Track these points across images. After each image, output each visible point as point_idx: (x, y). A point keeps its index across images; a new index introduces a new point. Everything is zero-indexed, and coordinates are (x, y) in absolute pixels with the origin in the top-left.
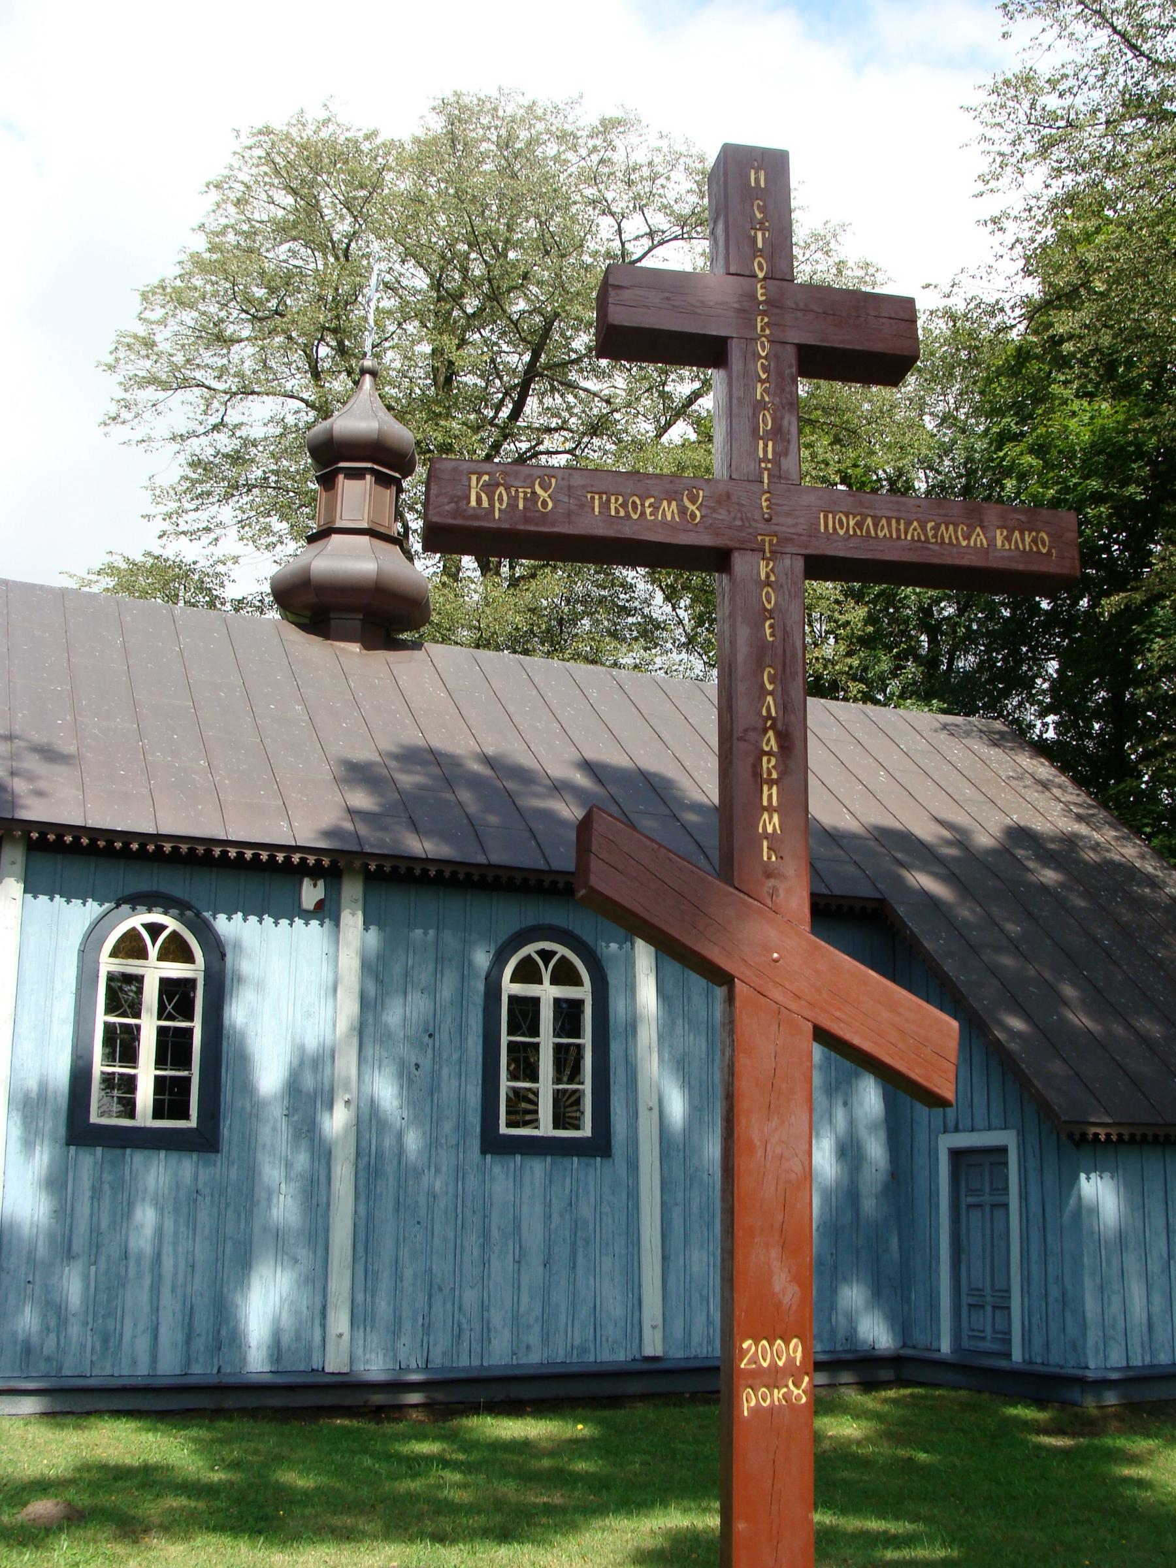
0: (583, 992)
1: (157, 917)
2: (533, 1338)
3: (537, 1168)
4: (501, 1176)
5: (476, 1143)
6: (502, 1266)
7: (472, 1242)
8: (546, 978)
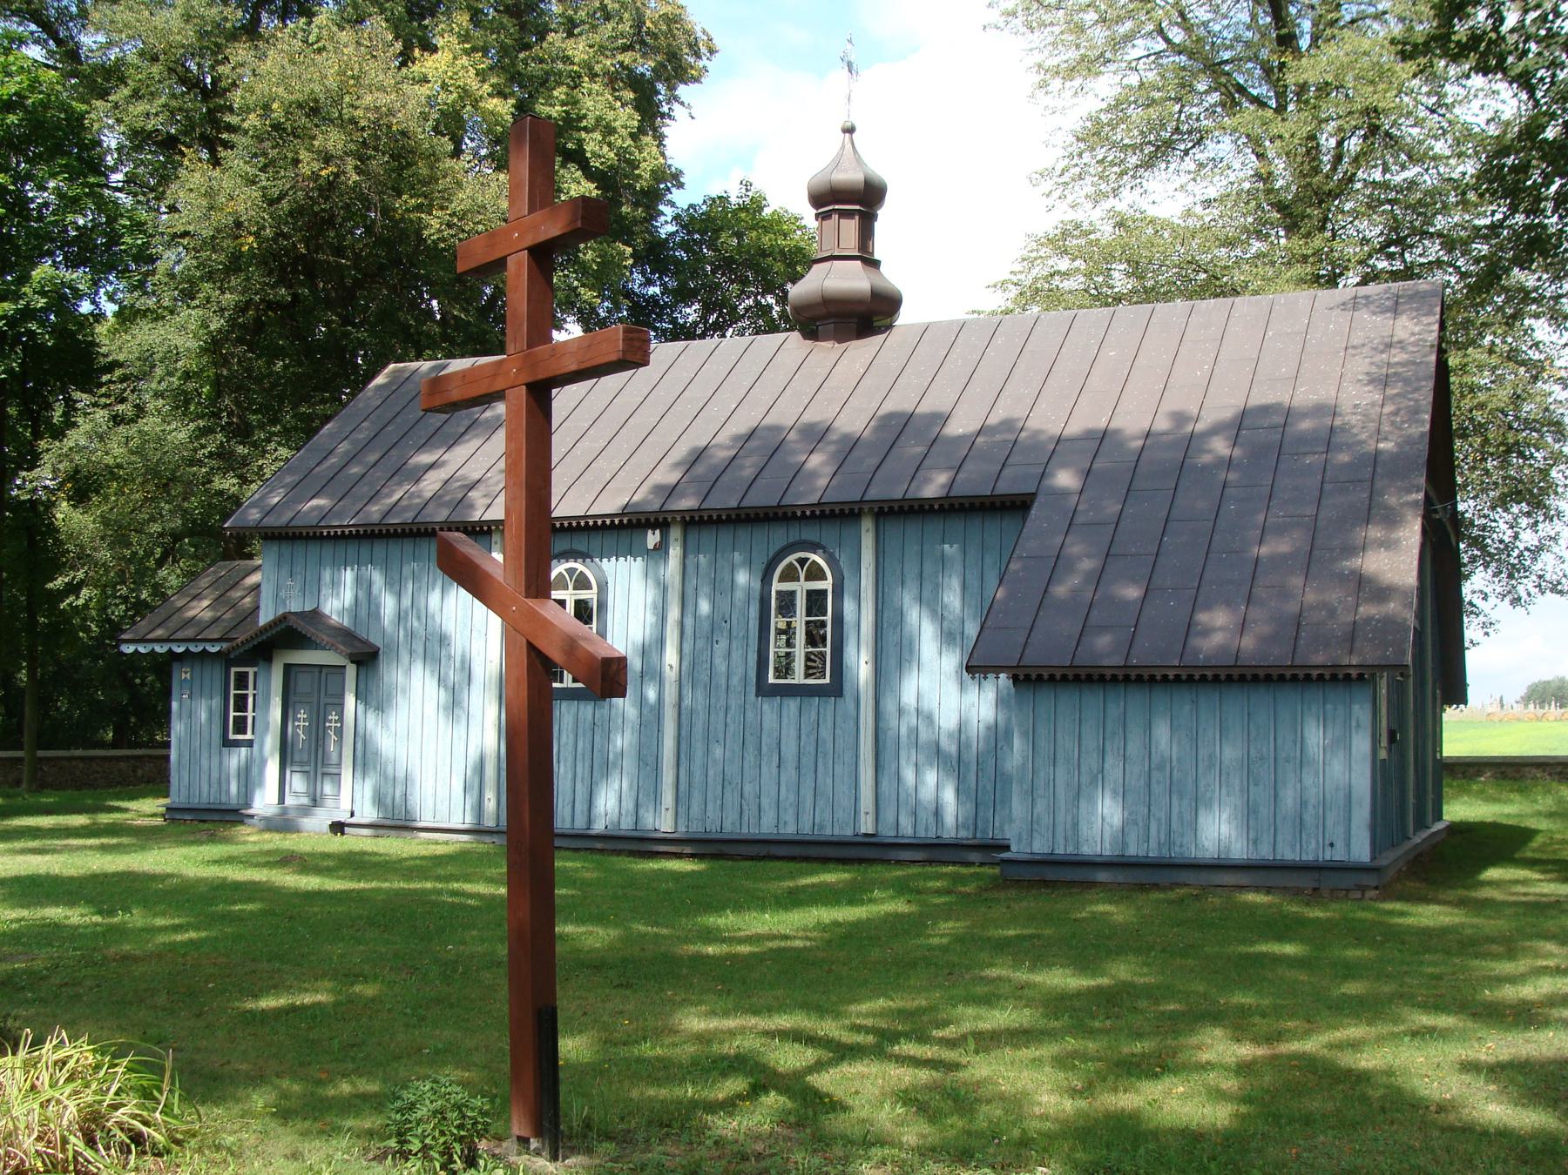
0: (826, 585)
1: (571, 564)
2: (789, 817)
3: (792, 705)
4: (769, 707)
5: (752, 689)
6: (769, 770)
7: (750, 758)
8: (571, 586)
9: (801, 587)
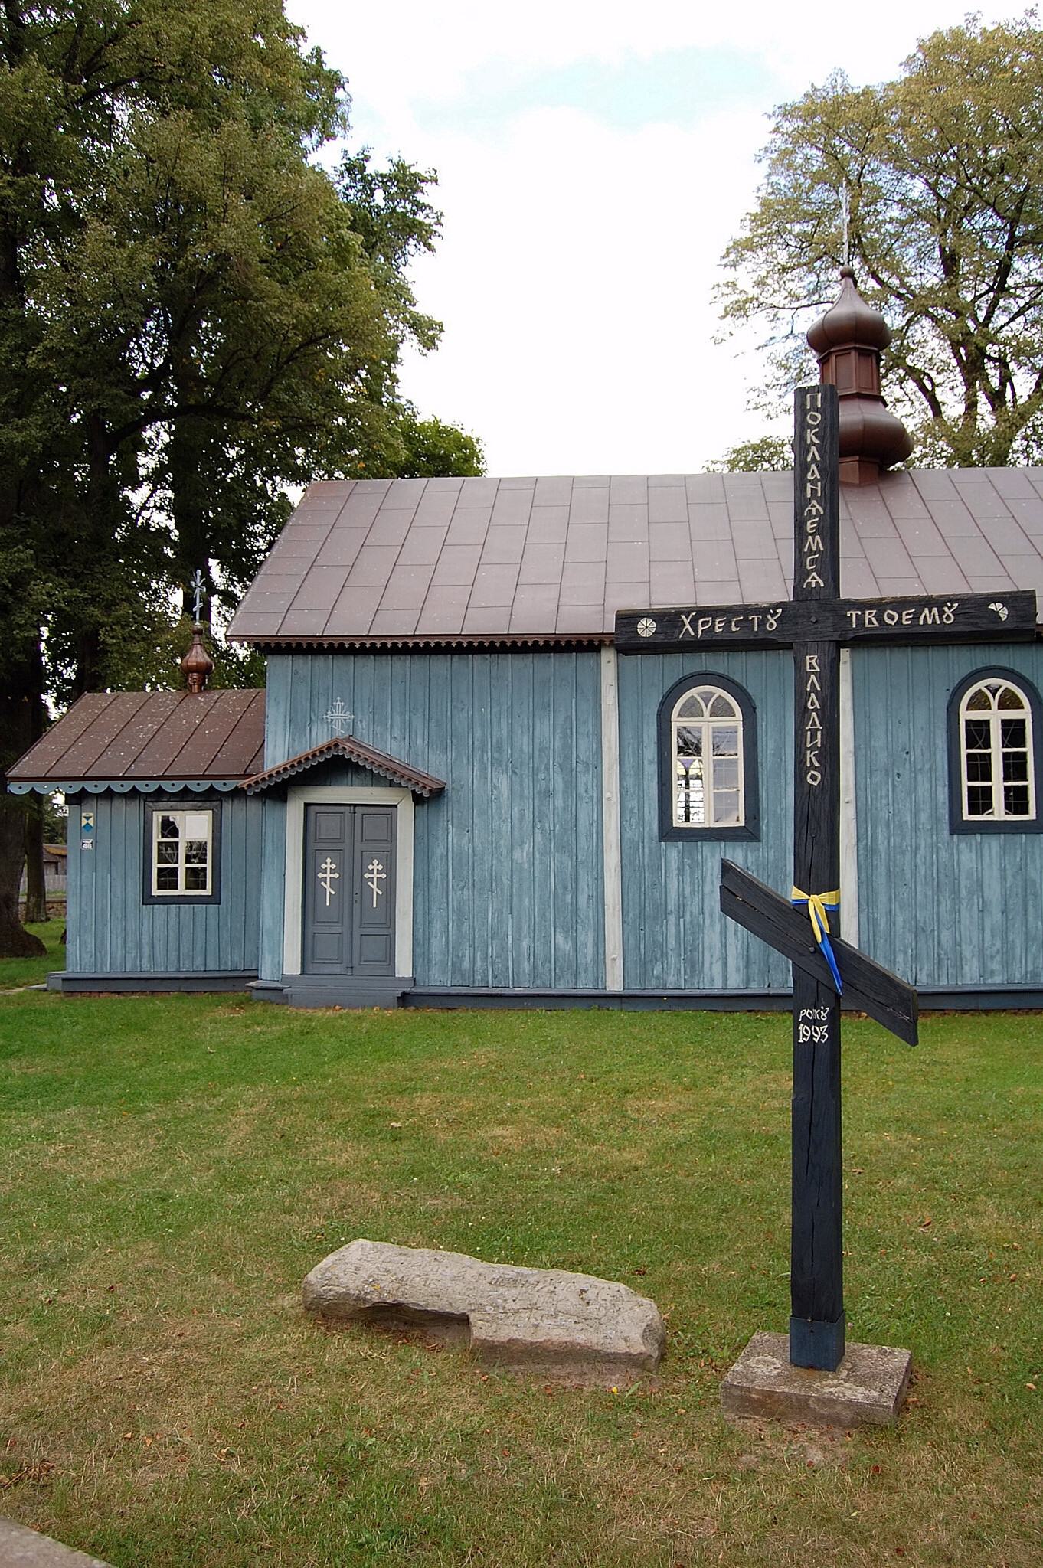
3: (994, 844)
4: (966, 852)
6: (968, 918)
9: (995, 717)
